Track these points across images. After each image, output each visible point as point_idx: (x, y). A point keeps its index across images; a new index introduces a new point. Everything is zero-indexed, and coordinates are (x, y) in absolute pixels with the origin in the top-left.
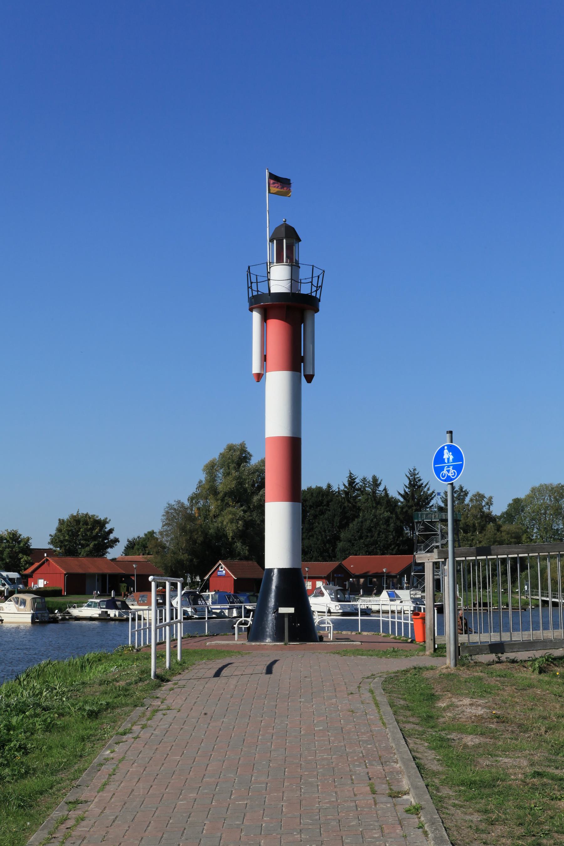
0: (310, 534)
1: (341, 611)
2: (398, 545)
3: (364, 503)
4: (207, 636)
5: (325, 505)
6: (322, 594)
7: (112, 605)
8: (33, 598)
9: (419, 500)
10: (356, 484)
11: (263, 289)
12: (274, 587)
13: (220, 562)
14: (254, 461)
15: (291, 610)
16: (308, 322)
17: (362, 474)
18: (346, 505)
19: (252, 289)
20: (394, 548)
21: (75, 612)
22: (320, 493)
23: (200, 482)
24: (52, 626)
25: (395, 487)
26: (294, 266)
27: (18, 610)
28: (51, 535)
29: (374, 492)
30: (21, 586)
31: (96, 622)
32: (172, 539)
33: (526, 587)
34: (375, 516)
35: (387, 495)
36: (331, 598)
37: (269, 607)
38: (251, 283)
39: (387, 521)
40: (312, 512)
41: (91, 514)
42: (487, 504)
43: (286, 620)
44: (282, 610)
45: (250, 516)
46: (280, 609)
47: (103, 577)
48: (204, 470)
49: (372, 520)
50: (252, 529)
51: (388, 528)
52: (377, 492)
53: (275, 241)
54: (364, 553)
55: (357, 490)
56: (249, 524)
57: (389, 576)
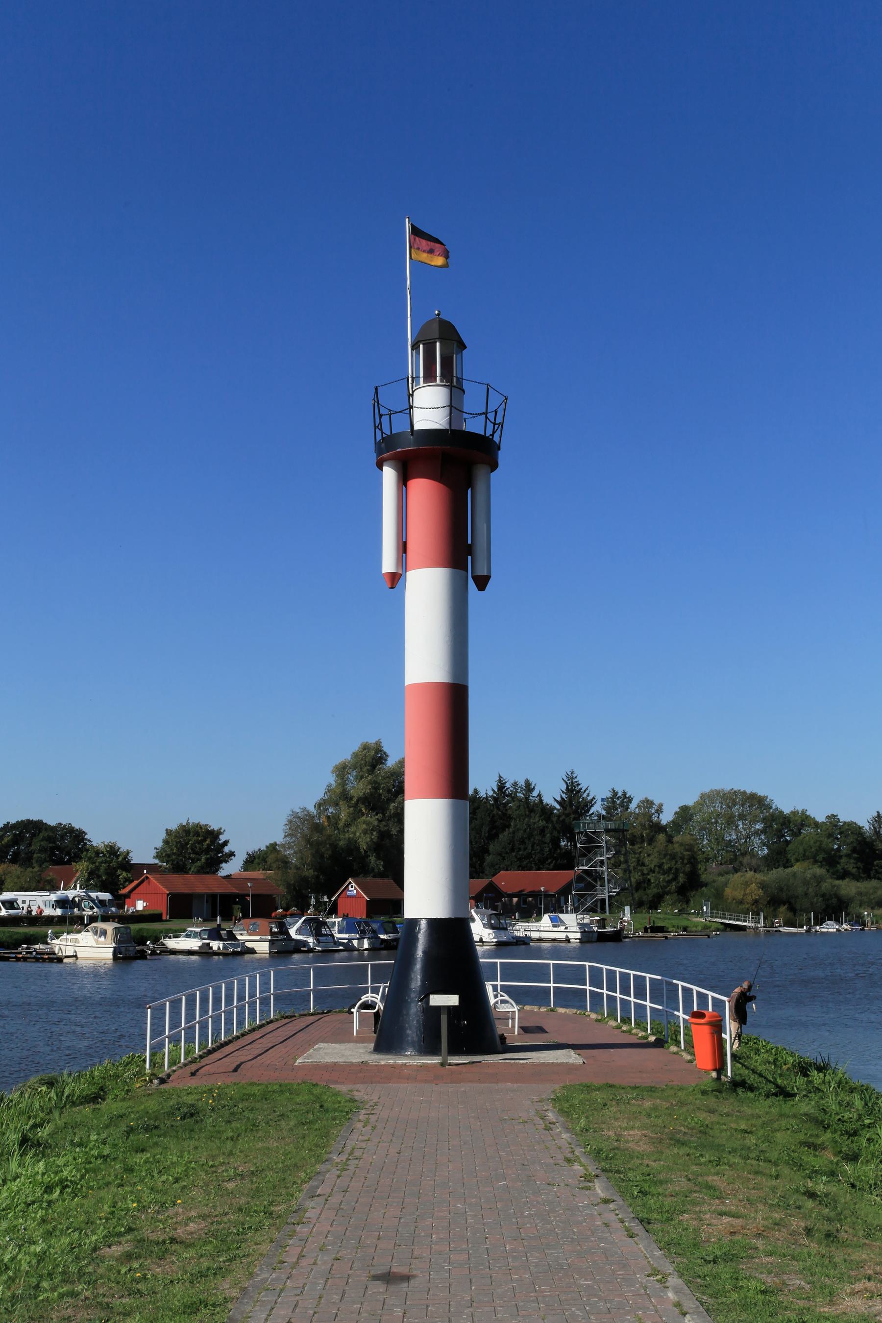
1: (495, 940)
4: (312, 1014)
7: (215, 934)
8: (115, 928)
9: (577, 808)
11: (399, 426)
12: (420, 953)
13: (350, 880)
14: (391, 763)
15: (453, 1000)
16: (480, 486)
18: (495, 812)
19: (381, 430)
20: (551, 862)
21: (171, 944)
23: (329, 786)
24: (139, 963)
26: (455, 387)
27: (97, 942)
28: (156, 848)
29: (527, 799)
30: (113, 909)
31: (194, 958)
32: (295, 853)
34: (529, 826)
35: (541, 801)
37: (411, 989)
38: (381, 416)
39: (542, 831)
41: (203, 823)
42: (657, 811)
43: (444, 1019)
44: (436, 1000)
46: (432, 996)
47: (213, 897)
48: (333, 772)
49: (525, 830)
53: (421, 346)
55: (508, 796)
56: (384, 835)
57: (547, 895)
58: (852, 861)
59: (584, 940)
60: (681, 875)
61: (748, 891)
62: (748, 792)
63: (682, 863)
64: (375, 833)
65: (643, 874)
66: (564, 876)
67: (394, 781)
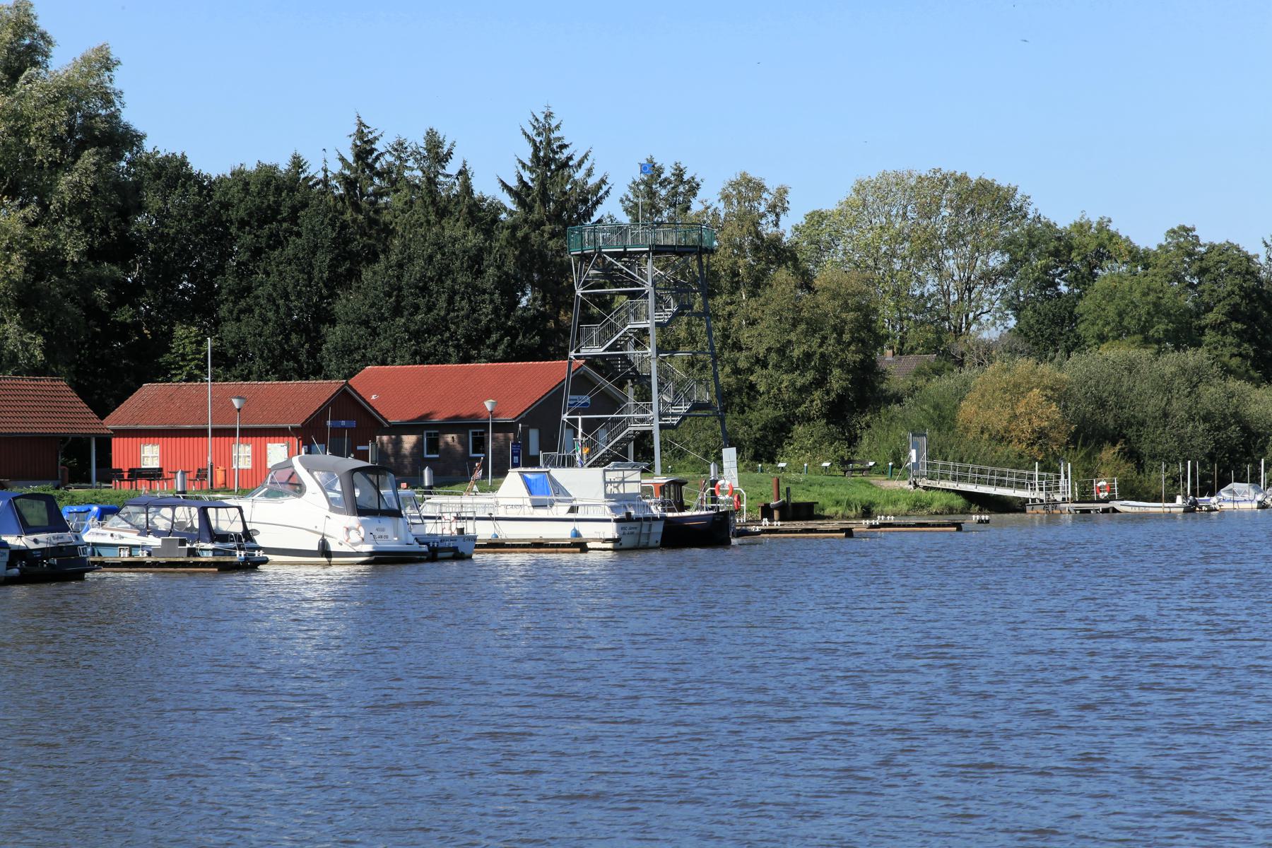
0: (242, 304)
1: (368, 548)
2: (510, 332)
3: (403, 211)
5: (284, 220)
6: (297, 488)
9: (561, 206)
10: (377, 158)
14: (61, 61)
17: (399, 129)
18: (348, 216)
20: (499, 341)
22: (268, 184)
25: (493, 168)
29: (431, 181)
33: (913, 453)
35: (467, 189)
36: (330, 500)
39: (476, 261)
40: (248, 239)
42: (773, 208)
45: (47, 237)
49: (431, 258)
50: (55, 278)
51: (478, 282)
52: (441, 178)
54: (408, 357)
58: (1229, 339)
59: (627, 542)
60: (836, 372)
61: (1021, 409)
62: (974, 177)
63: (839, 341)
64: (15, 257)
65: (736, 371)
66: (542, 376)
67: (71, 111)
